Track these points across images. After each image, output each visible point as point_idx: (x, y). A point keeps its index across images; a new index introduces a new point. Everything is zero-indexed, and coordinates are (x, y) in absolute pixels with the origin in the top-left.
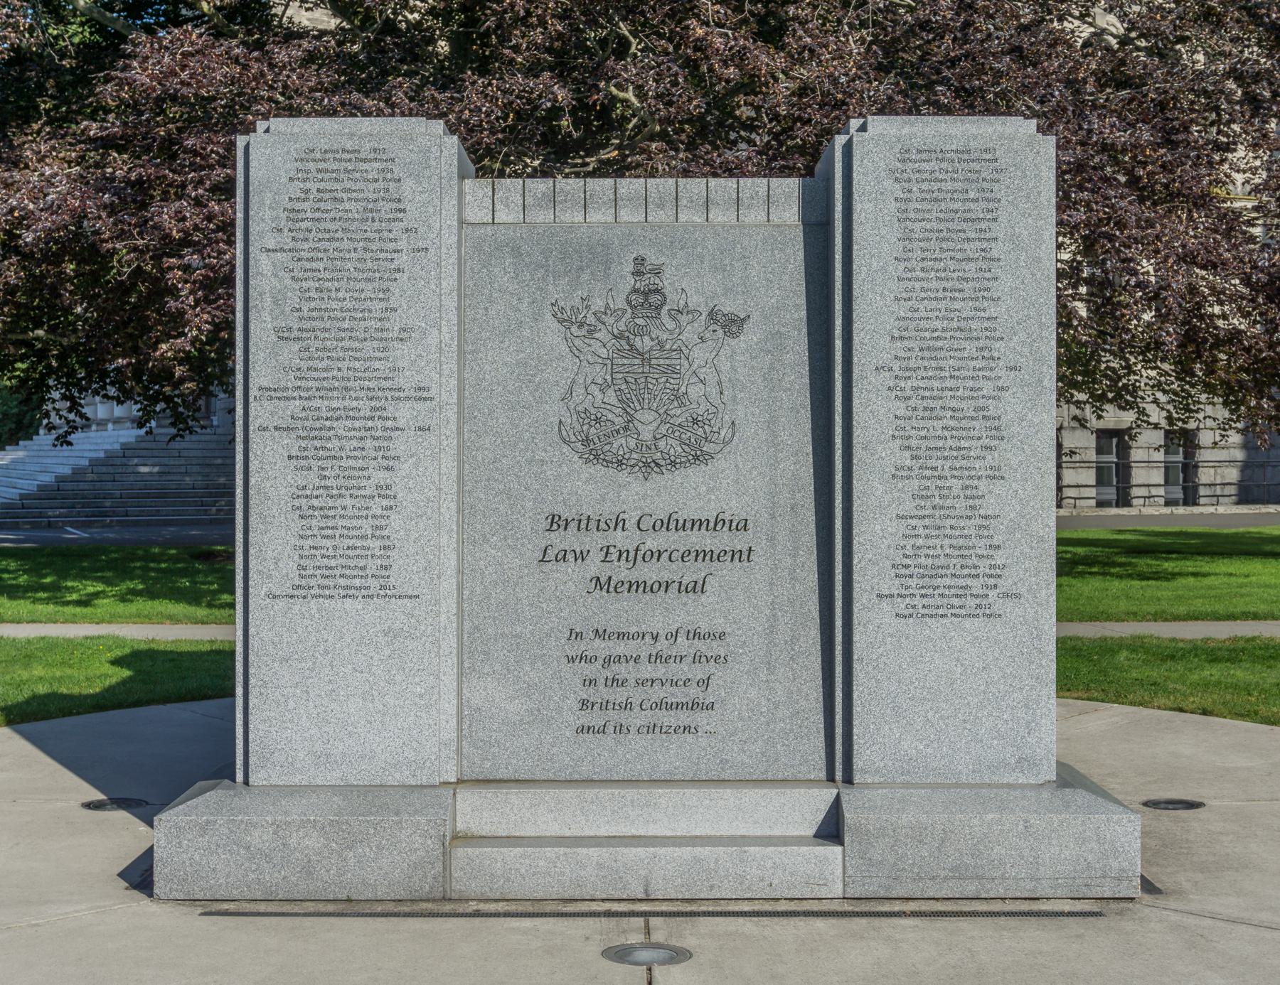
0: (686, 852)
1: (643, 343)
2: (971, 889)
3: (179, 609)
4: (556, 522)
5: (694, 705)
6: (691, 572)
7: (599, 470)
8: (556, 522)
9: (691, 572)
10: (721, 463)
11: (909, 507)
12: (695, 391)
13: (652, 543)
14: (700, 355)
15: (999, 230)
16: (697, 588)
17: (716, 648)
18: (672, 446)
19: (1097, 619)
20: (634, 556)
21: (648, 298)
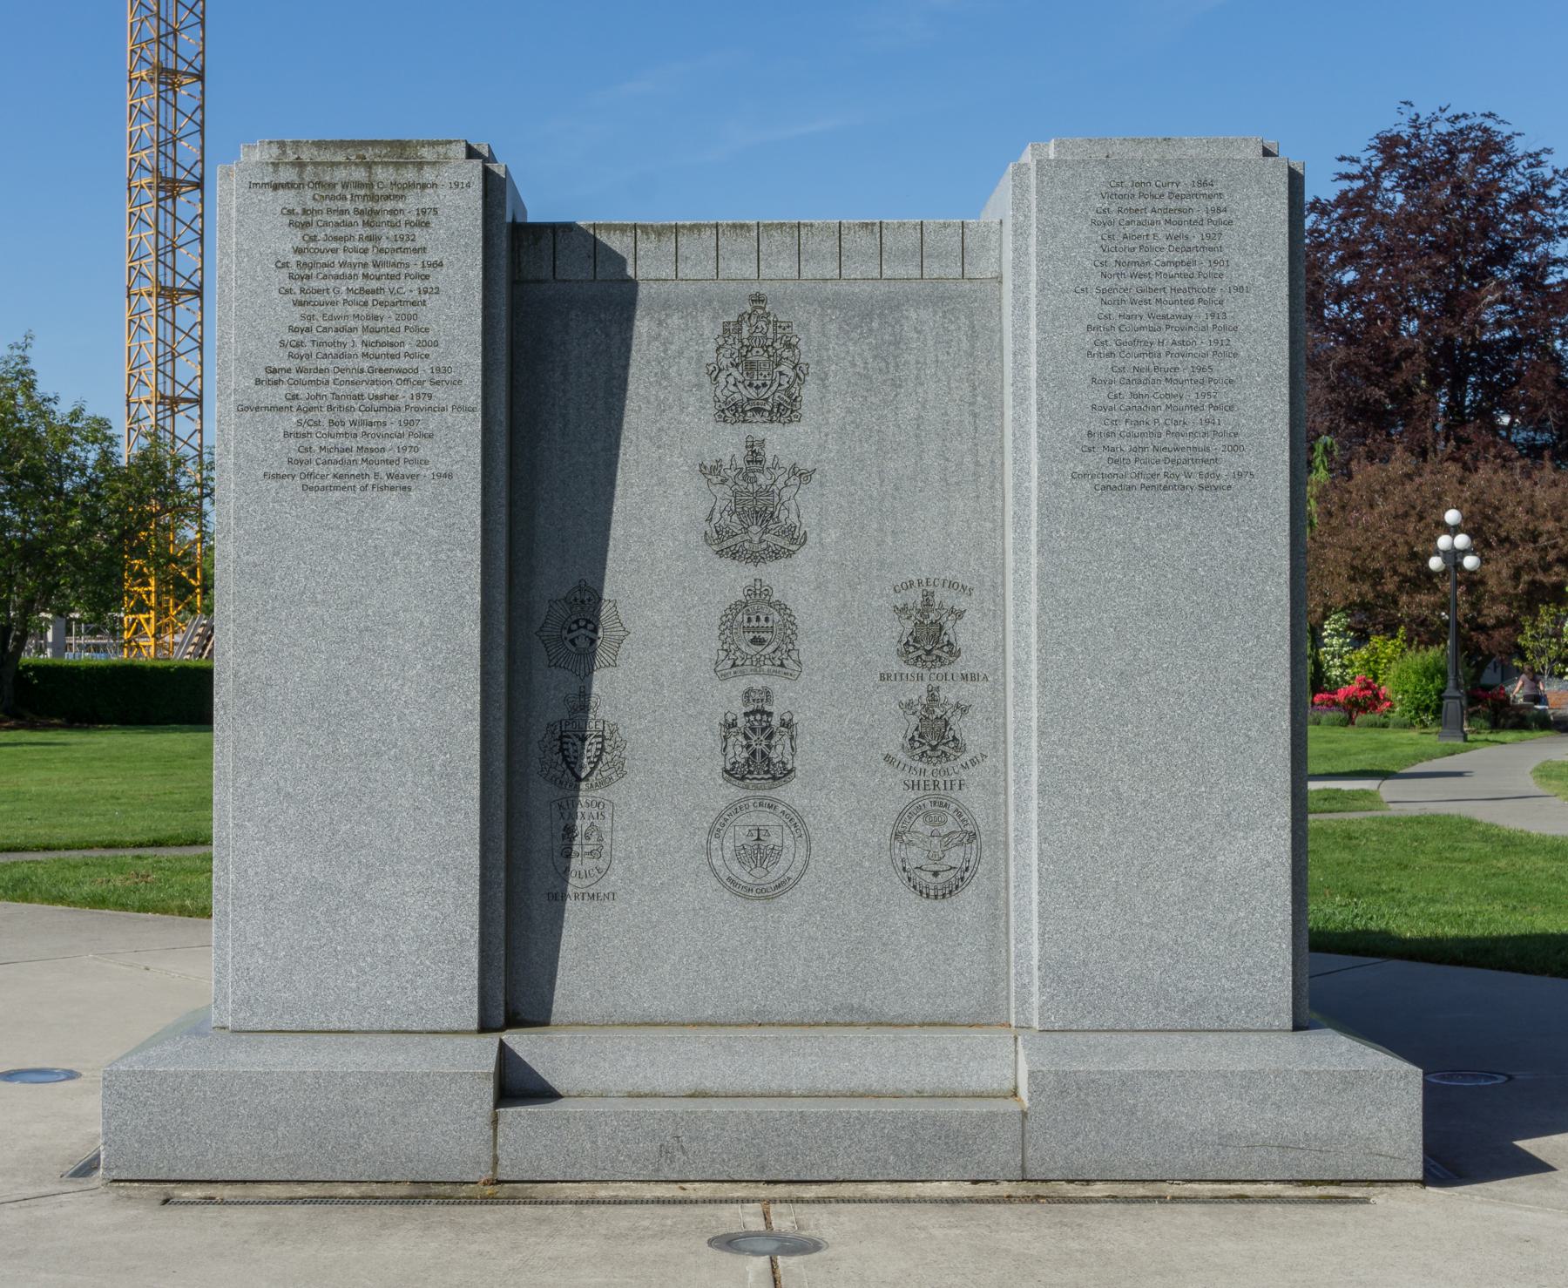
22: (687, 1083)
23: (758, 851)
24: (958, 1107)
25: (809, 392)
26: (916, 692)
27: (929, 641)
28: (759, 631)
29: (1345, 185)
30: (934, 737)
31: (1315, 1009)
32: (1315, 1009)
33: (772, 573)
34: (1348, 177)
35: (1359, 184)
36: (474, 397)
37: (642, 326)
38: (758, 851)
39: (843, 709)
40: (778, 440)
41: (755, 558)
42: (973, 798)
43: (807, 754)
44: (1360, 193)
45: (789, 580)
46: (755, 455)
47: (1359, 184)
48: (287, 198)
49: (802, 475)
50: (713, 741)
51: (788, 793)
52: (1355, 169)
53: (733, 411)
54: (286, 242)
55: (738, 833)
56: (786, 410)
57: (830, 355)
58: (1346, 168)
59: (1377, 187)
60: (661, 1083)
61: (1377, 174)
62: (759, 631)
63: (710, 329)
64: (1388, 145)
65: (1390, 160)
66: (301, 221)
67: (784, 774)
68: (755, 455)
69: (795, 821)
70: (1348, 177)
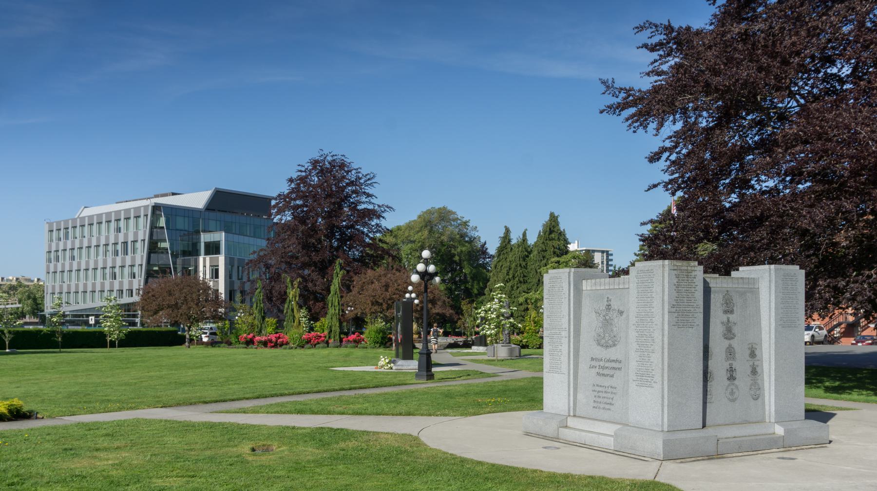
0: (590, 435)
1: (607, 318)
2: (633, 452)
3: (773, 341)
4: (592, 359)
5: (611, 404)
6: (611, 372)
7: (599, 347)
8: (592, 359)
9: (611, 372)
10: (618, 346)
11: (638, 359)
12: (615, 329)
13: (606, 365)
14: (616, 320)
15: (654, 290)
16: (612, 376)
17: (614, 391)
18: (610, 342)
19: (258, 412)
20: (603, 368)
21: (609, 307)
22: (733, 435)
23: (732, 393)
24: (758, 437)
25: (735, 308)
26: (751, 363)
27: (753, 355)
28: (730, 353)
29: (299, 173)
30: (754, 372)
31: (807, 417)
32: (807, 417)
33: (732, 342)
34: (301, 171)
35: (304, 174)
36: (702, 311)
37: (712, 296)
38: (732, 393)
39: (742, 367)
40: (732, 317)
41: (730, 339)
42: (759, 382)
43: (738, 375)
44: (306, 177)
45: (735, 343)
46: (728, 319)
47: (304, 174)
48: (675, 272)
49: (735, 324)
50: (725, 373)
51: (736, 382)
52: (303, 169)
53: (726, 312)
54: (675, 281)
55: (729, 390)
56: (732, 312)
57: (737, 300)
58: (300, 168)
59: (310, 174)
60: (729, 436)
61: (310, 171)
62: (730, 353)
63: (721, 297)
64: (315, 163)
65: (314, 168)
66: (677, 276)
67: (735, 379)
68: (728, 319)
69: (737, 387)
70: (301, 171)
